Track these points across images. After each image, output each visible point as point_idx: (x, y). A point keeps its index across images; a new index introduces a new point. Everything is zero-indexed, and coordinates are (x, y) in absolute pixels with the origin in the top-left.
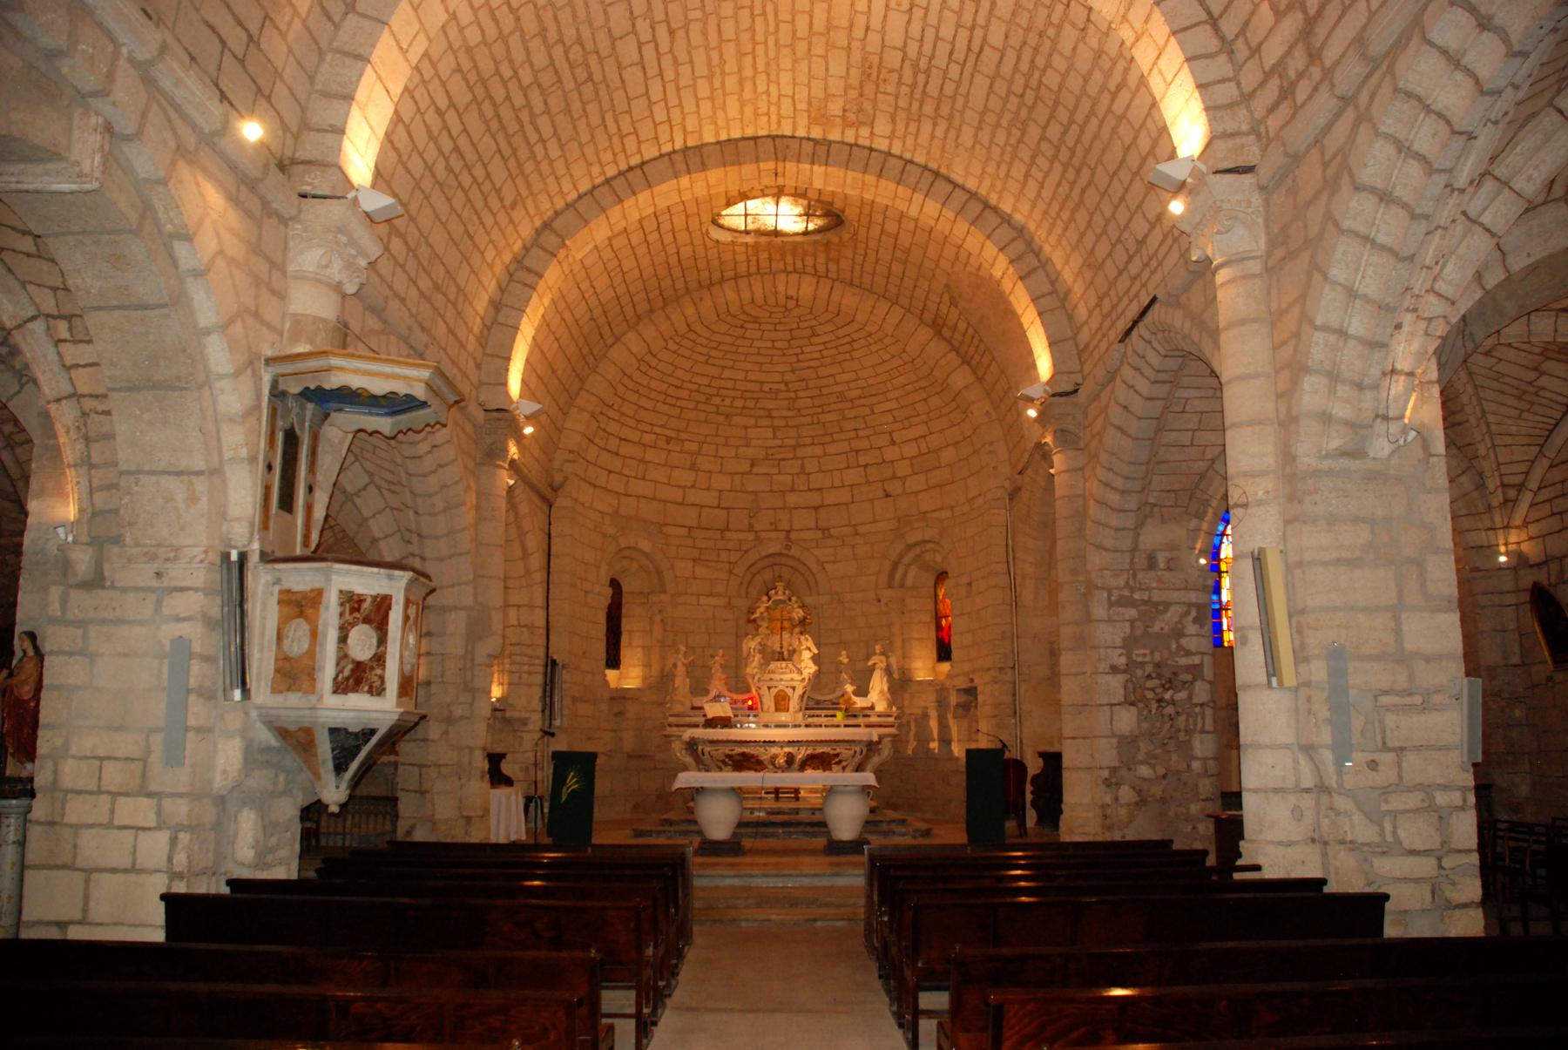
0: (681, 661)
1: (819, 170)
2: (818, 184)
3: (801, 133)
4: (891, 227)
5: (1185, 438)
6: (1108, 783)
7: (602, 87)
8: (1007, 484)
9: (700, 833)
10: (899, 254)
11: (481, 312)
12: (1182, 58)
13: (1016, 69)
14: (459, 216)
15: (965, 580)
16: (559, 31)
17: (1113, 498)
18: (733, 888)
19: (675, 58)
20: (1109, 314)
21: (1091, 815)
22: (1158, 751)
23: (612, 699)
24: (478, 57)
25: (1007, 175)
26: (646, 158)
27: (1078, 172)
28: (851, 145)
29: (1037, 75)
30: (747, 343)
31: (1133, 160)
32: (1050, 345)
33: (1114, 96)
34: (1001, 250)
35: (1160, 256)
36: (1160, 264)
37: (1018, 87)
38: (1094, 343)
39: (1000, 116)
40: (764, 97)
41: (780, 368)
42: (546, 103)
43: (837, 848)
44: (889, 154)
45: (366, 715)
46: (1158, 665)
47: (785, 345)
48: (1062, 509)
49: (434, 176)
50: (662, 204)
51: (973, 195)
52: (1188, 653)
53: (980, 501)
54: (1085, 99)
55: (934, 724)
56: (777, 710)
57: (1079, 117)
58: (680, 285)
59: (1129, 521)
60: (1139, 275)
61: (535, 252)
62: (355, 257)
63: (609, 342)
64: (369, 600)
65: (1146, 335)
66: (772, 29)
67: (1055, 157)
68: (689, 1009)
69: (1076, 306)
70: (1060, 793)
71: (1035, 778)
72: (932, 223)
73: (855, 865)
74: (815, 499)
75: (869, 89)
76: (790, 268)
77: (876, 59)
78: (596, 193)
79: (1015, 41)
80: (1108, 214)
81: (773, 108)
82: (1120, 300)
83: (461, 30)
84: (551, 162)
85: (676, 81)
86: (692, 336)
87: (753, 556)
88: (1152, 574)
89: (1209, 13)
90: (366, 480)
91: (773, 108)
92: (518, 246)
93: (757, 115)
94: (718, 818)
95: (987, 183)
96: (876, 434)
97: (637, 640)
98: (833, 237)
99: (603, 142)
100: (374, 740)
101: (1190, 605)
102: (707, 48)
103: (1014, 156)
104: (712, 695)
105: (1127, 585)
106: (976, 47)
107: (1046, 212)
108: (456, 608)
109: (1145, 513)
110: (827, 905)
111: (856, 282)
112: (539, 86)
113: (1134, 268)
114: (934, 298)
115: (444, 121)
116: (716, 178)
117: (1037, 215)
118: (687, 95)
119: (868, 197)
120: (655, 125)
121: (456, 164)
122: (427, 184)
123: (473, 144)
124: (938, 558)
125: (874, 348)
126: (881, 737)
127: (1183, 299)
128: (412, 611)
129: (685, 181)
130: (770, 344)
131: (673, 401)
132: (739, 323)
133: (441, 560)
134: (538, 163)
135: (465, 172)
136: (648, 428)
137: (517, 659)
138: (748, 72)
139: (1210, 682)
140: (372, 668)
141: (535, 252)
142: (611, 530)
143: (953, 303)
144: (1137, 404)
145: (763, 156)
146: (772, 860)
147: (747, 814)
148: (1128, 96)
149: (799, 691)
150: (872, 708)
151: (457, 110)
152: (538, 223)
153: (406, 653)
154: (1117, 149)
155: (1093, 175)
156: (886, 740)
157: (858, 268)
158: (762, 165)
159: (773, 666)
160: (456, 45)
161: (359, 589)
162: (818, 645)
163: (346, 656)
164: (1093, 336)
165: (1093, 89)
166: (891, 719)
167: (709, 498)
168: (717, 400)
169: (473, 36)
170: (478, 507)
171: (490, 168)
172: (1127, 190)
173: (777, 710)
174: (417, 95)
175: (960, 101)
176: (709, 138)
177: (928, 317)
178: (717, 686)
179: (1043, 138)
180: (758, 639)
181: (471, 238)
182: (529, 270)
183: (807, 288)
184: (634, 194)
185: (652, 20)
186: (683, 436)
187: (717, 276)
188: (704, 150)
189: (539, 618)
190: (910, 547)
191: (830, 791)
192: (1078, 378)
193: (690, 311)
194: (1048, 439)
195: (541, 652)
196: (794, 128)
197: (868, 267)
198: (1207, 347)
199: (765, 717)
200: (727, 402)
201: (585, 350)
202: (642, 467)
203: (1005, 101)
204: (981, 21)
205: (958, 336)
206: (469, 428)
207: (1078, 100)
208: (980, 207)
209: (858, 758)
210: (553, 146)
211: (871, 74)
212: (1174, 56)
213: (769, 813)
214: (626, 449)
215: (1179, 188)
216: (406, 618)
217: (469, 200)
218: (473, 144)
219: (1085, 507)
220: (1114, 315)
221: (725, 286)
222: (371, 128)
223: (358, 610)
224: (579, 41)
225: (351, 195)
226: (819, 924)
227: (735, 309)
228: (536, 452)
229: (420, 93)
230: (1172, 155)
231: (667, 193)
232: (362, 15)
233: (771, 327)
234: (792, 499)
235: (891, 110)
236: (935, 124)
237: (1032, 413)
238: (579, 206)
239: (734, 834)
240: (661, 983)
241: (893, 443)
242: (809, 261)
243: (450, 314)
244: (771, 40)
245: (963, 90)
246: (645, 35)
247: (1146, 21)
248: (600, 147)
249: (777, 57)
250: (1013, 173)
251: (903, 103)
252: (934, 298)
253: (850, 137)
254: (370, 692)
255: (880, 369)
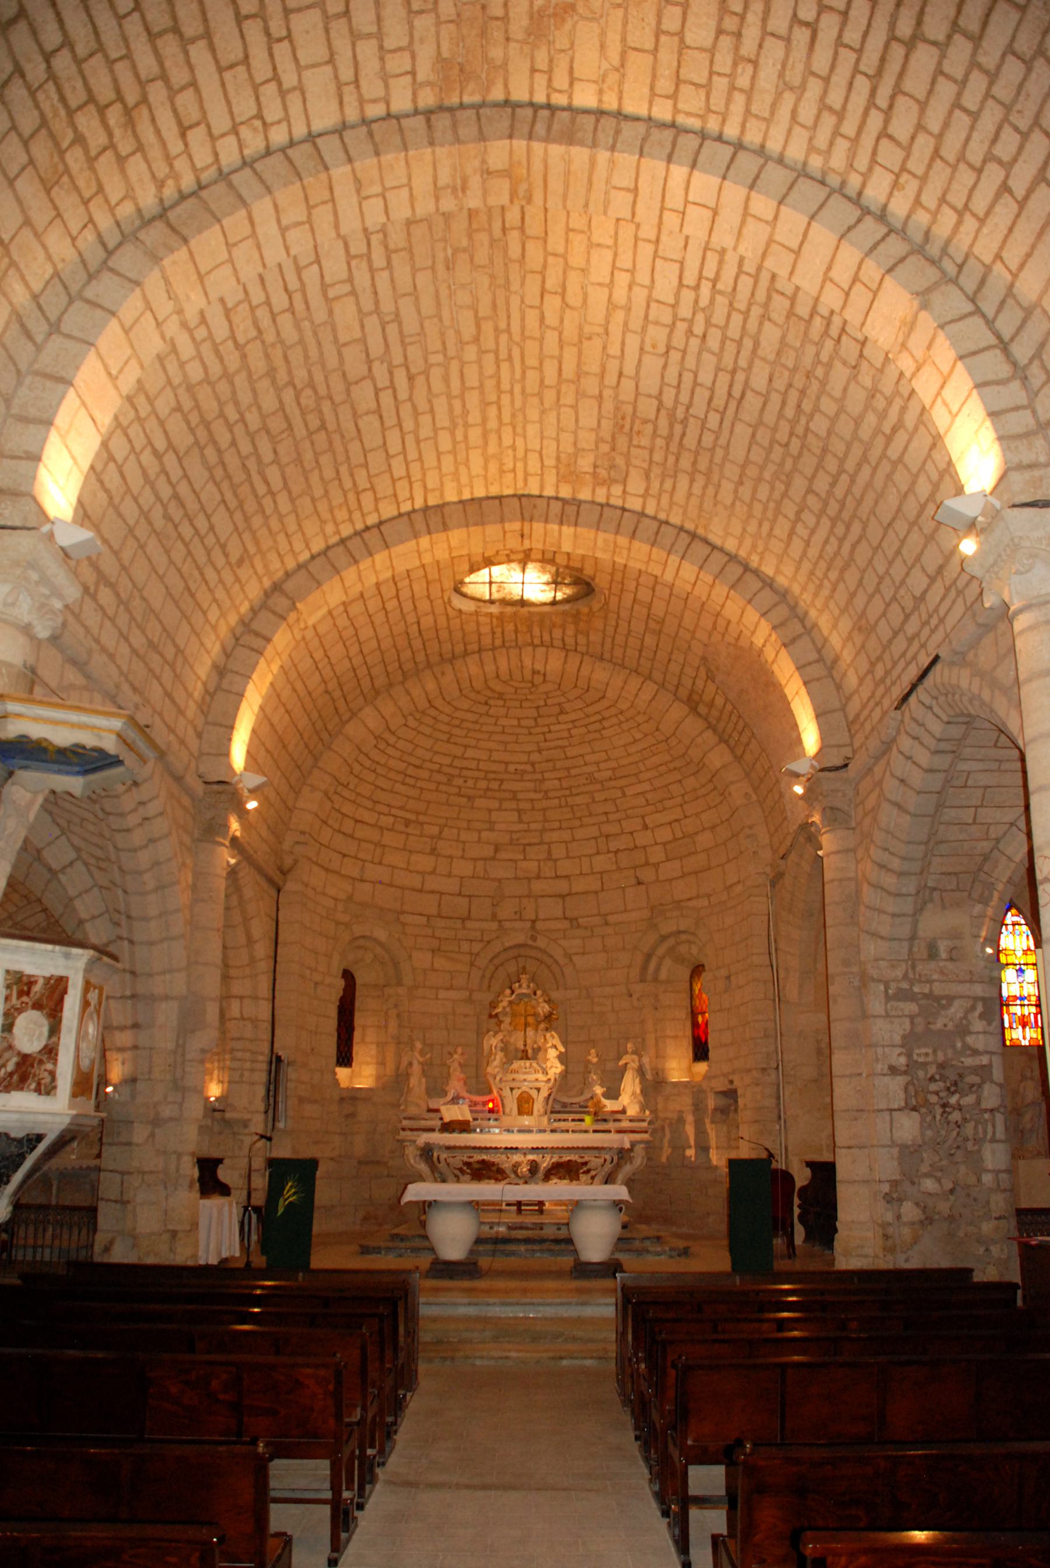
0: (417, 1058)
1: (567, 531)
2: (567, 547)
3: (549, 492)
4: (644, 595)
5: (967, 815)
6: (888, 1198)
7: (336, 437)
8: (768, 870)
9: (432, 1250)
10: (652, 625)
11: (204, 677)
12: (971, 384)
13: (781, 415)
14: (179, 570)
15: (723, 972)
16: (290, 372)
17: (889, 881)
18: (467, 1319)
19: (414, 407)
20: (883, 680)
21: (870, 1234)
22: (944, 1163)
23: (342, 1099)
24: (201, 397)
25: (770, 534)
26: (384, 517)
27: (848, 527)
28: (602, 506)
29: (803, 421)
30: (492, 721)
31: (911, 508)
32: (817, 717)
33: (889, 439)
34: (763, 615)
35: (942, 613)
36: (942, 621)
37: (782, 436)
38: (866, 713)
39: (762, 468)
40: (510, 452)
41: (528, 748)
42: (275, 452)
43: (583, 1270)
44: (643, 514)
45: (31, 1117)
46: (942, 1066)
47: (531, 723)
48: (832, 893)
49: (150, 524)
50: (401, 567)
51: (732, 558)
52: (975, 1052)
53: (739, 888)
54: (856, 444)
55: (690, 1130)
56: (520, 1113)
57: (850, 465)
58: (421, 657)
59: (907, 906)
60: (917, 635)
61: (264, 615)
62: (48, 597)
63: (345, 718)
64: (41, 982)
65: (928, 701)
66: (518, 376)
67: (823, 511)
68: (408, 1484)
69: (845, 674)
70: (834, 1208)
71: (803, 1189)
72: (689, 588)
73: (606, 1292)
74: (562, 886)
75: (622, 442)
76: (537, 641)
77: (629, 409)
78: (330, 554)
79: (780, 384)
80: (881, 570)
81: (520, 465)
82: (895, 664)
83: (182, 365)
84: (281, 518)
85: (416, 432)
86: (432, 712)
87: (496, 946)
88: (932, 965)
89: (999, 337)
90: (73, 855)
91: (520, 465)
92: (244, 608)
93: (502, 472)
94: (453, 1236)
95: (748, 542)
96: (628, 817)
97: (371, 1035)
98: (583, 607)
99: (337, 498)
100: (42, 1147)
101: (976, 999)
102: (449, 397)
103: (778, 512)
104: (450, 1097)
105: (905, 976)
106: (737, 393)
107: (812, 573)
108: (166, 998)
109: (925, 897)
110: (574, 1339)
111: (607, 656)
112: (268, 432)
113: (911, 628)
114: (689, 671)
115: (162, 464)
116: (459, 540)
117: (802, 578)
118: (427, 448)
119: (620, 560)
120: (394, 481)
121: (176, 514)
122: (142, 532)
123: (194, 491)
124: (694, 951)
125: (625, 726)
126: (633, 1144)
127: (970, 656)
128: (93, 996)
129: (425, 541)
130: (515, 722)
131: (412, 781)
132: (483, 699)
133: (152, 944)
134: (266, 518)
135: (186, 523)
136: (386, 810)
137: (239, 1055)
138: (492, 424)
139: (1000, 1085)
140: (41, 1062)
141: (264, 615)
142: (346, 918)
143: (710, 677)
144: (917, 778)
145: (507, 516)
146: (513, 1284)
147: (486, 1228)
148: (906, 437)
149: (544, 1093)
150: (623, 1111)
151: (176, 452)
152: (267, 583)
153: (83, 1045)
154: (892, 499)
155: (864, 529)
156: (639, 1149)
157: (609, 640)
158: (507, 526)
159: (517, 1064)
160: (176, 381)
161: (29, 970)
162: (564, 1043)
163: (10, 1047)
164: (864, 706)
165: (865, 433)
166: (645, 1124)
167: (450, 885)
168: (459, 782)
169: (195, 372)
170: (194, 888)
171: (214, 519)
172: (903, 542)
173: (520, 1113)
174: (131, 432)
175: (719, 453)
176: (451, 497)
177: (683, 693)
178: (455, 1086)
179: (810, 491)
180: (500, 1036)
181: (192, 595)
182: (257, 634)
183: (555, 663)
184: (371, 554)
185: (390, 364)
186: (422, 818)
187: (459, 649)
188: (446, 510)
189: (264, 1011)
190: (664, 938)
191: (576, 1206)
192: (847, 752)
193: (431, 686)
194: (816, 818)
195: (266, 1048)
196: (542, 488)
197: (620, 639)
198: (1001, 707)
199: (506, 1121)
200: (470, 783)
201: (319, 725)
202: (379, 851)
203: (769, 450)
204: (742, 363)
205: (715, 713)
206: (186, 801)
207: (849, 446)
208: (740, 570)
209: (608, 1167)
210: (282, 499)
211: (624, 425)
212: (961, 381)
213: (510, 1228)
214: (361, 832)
215: (971, 526)
216: (86, 1004)
217: (190, 553)
218: (194, 491)
219: (858, 891)
220: (888, 681)
221: (468, 659)
222: (73, 458)
223: (28, 993)
224: (312, 385)
225: (45, 529)
226: (565, 1362)
227: (478, 685)
228: (264, 832)
229: (135, 431)
230: (959, 490)
231: (407, 556)
232: (68, 336)
233: (517, 704)
234: (537, 886)
235: (645, 465)
236: (692, 481)
237: (799, 790)
238: (311, 567)
239: (472, 1252)
240: (370, 1452)
241: (646, 827)
242: (557, 633)
243: (167, 676)
244: (517, 389)
245: (723, 441)
246: (383, 381)
247: (929, 347)
248: (335, 503)
249: (523, 409)
250: (777, 532)
251: (658, 457)
252: (689, 671)
253: (601, 496)
254: (38, 1090)
255: (632, 749)
